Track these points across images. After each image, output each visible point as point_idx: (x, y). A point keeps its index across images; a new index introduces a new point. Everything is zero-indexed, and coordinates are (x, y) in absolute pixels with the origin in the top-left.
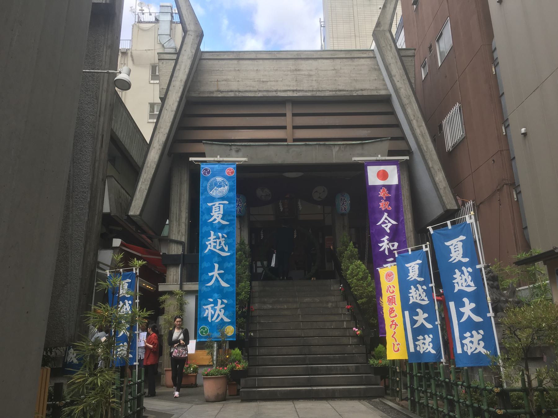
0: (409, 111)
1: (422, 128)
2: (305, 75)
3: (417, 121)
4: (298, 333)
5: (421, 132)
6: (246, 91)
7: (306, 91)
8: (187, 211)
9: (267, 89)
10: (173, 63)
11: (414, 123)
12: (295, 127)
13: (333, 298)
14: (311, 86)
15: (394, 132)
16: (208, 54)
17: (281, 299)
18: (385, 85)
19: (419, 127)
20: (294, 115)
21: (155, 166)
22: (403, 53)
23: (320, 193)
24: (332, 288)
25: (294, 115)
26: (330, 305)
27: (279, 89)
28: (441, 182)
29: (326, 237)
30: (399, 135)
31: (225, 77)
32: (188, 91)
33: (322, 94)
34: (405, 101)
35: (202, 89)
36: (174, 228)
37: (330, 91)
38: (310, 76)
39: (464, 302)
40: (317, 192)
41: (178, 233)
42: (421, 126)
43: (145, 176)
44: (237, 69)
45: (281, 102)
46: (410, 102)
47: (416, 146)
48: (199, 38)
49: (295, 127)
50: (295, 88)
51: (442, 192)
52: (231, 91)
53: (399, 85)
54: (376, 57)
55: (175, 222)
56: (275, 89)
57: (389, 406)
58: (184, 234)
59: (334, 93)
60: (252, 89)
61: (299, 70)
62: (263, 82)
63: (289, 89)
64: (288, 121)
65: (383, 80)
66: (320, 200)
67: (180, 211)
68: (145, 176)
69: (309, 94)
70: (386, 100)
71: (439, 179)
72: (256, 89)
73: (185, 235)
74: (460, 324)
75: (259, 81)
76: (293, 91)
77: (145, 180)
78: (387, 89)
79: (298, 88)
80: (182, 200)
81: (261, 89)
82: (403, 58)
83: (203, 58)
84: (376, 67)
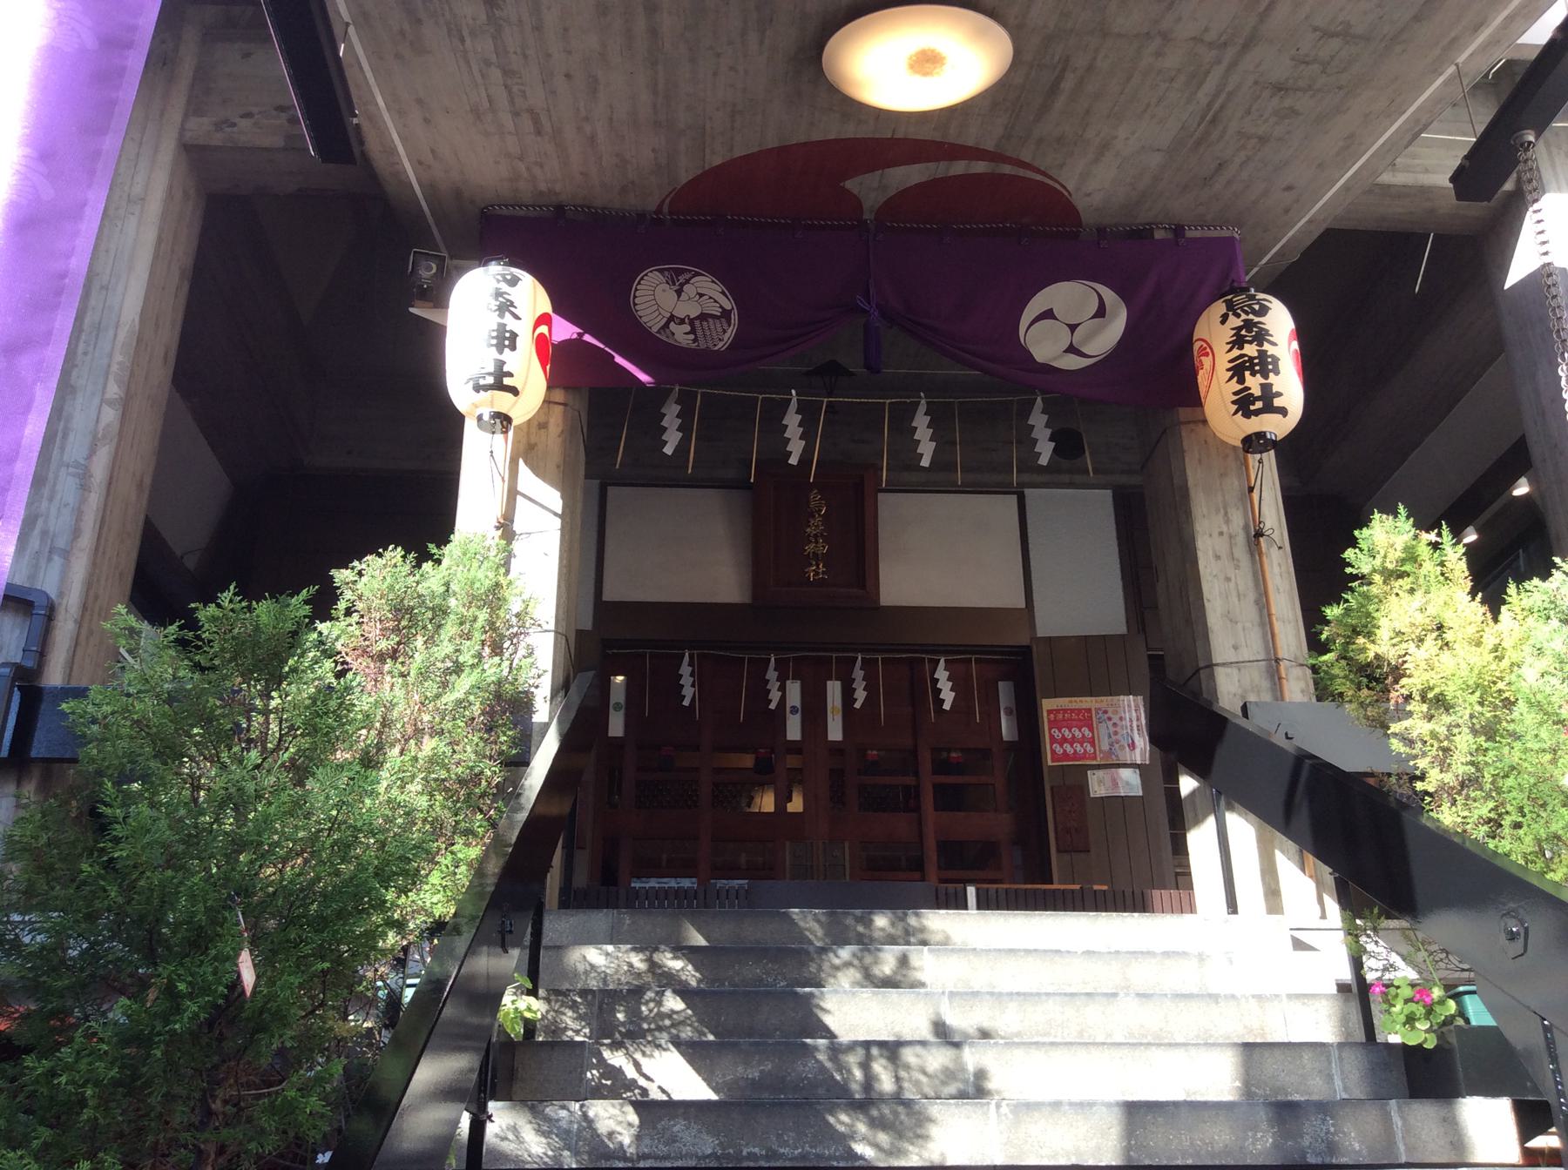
29: (1048, 704)
40: (1048, 314)
66: (1073, 363)
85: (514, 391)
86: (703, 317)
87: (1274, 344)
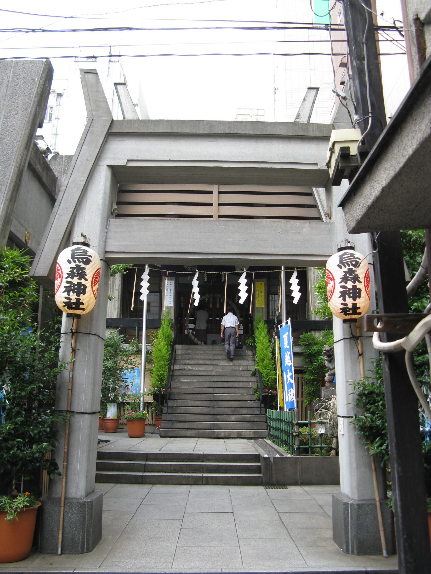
4: (210, 390)
8: (120, 279)
12: (220, 204)
24: (246, 353)
25: (220, 192)
30: (317, 215)
49: (220, 204)
58: (117, 299)
64: (215, 198)
73: (118, 301)
85: (83, 309)
87: (86, 280)
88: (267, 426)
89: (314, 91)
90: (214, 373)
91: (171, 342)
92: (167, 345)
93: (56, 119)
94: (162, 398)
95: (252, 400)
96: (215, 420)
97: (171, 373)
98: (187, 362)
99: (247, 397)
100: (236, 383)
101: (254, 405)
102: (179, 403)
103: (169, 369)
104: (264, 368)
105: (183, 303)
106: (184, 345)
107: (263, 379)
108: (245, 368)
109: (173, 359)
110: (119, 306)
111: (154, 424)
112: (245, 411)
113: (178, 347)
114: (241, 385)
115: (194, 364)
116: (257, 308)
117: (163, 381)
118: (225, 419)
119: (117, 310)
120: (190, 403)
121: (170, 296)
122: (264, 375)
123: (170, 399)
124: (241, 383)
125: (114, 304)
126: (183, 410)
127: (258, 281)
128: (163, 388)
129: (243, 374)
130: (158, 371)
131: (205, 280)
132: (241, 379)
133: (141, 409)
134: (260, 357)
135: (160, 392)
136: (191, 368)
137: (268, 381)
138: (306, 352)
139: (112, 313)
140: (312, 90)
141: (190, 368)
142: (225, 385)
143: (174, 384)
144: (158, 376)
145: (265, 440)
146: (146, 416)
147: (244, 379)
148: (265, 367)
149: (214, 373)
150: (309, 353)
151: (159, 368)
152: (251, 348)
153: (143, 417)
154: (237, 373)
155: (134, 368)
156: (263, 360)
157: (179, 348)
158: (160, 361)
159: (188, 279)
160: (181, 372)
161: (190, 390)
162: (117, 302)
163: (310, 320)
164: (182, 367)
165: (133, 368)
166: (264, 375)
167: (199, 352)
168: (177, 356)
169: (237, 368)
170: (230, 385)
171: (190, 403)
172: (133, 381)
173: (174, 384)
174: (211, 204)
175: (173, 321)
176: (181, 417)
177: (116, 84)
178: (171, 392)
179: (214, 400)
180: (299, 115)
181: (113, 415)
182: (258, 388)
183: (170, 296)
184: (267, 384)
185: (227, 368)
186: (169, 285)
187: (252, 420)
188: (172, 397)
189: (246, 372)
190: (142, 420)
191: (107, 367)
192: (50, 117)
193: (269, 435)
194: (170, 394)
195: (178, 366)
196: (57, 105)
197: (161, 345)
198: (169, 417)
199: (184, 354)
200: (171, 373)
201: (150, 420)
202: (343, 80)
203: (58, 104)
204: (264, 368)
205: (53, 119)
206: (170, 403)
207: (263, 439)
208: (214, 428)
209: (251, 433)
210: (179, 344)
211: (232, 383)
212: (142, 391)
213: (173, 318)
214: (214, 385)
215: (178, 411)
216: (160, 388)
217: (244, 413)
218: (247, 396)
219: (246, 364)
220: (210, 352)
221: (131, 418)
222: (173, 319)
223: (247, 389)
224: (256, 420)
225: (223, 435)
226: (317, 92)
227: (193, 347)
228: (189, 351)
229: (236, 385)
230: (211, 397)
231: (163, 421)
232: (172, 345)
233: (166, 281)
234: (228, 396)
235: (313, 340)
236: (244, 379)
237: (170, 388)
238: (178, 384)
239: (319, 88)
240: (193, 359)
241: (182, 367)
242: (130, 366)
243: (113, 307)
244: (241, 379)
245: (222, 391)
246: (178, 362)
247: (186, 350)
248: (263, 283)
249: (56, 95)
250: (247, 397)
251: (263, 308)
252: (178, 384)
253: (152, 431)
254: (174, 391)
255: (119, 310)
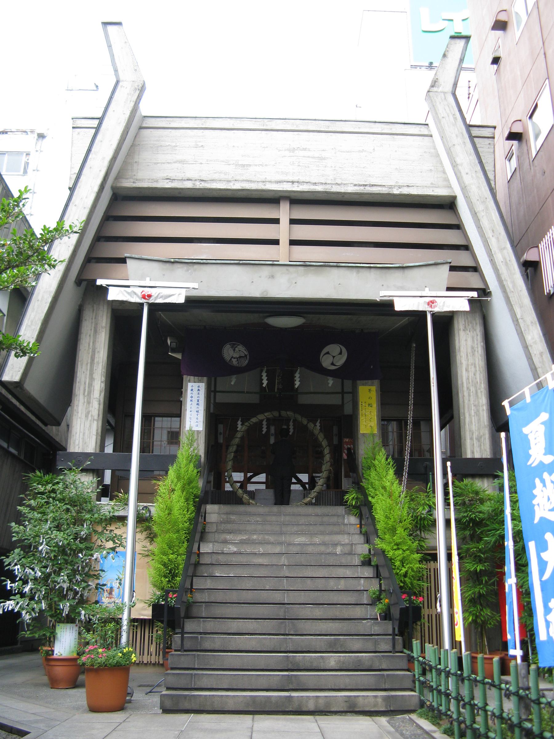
0: (485, 223)
1: (505, 251)
2: (313, 158)
3: (498, 239)
4: (277, 597)
5: (505, 258)
6: (213, 180)
7: (315, 184)
8: (103, 379)
9: (248, 178)
10: (93, 131)
11: (493, 242)
12: (293, 243)
13: (345, 539)
14: (323, 176)
15: (462, 259)
16: (154, 119)
17: (255, 537)
18: (447, 180)
19: (502, 249)
20: (293, 222)
21: (50, 300)
22: (475, 132)
23: (334, 356)
24: (346, 521)
25: (293, 222)
26: (338, 550)
27: (269, 179)
28: (535, 343)
30: (471, 263)
31: (179, 157)
32: (117, 178)
33: (342, 189)
34: (479, 208)
35: (140, 175)
36: (80, 408)
37: (355, 185)
38: (322, 159)
39: (546, 542)
40: (328, 353)
41: (87, 416)
42: (504, 248)
43: (32, 316)
44: (200, 144)
45: (272, 199)
46: (487, 208)
47: (496, 283)
48: (138, 92)
49: (293, 243)
50: (295, 179)
51: (536, 360)
52: (189, 180)
53: (467, 180)
54: (431, 136)
55: (81, 397)
56: (262, 178)
57: (421, 728)
58: (96, 418)
59: (362, 188)
60: (222, 177)
61: (305, 149)
62: (243, 166)
63: (286, 179)
64: (283, 231)
65: (444, 172)
66: (333, 368)
67: (92, 379)
68: (32, 316)
69: (319, 188)
70: (448, 205)
71: (533, 339)
72: (230, 178)
73: (98, 421)
74: (544, 585)
75: (237, 165)
76: (293, 182)
77: (32, 322)
78: (450, 187)
79: (302, 179)
80: (96, 360)
81: (237, 178)
82: (475, 139)
83: (144, 125)
84: (433, 151)
86: (240, 357)
88: (414, 682)
89: (462, 42)
90: (284, 560)
91: (196, 496)
92: (187, 500)
93: (34, 170)
94: (169, 616)
95: (370, 620)
96: (290, 667)
97: (194, 559)
98: (228, 537)
99: (358, 612)
100: (331, 580)
101: (376, 629)
102: (210, 626)
103: (189, 552)
104: (395, 547)
105: (222, 436)
106: (222, 506)
107: (394, 571)
108: (347, 549)
109: (197, 531)
110: (100, 431)
111: (161, 662)
112: (356, 644)
113: (210, 508)
114: (342, 584)
115: (242, 542)
116: (363, 434)
117: (174, 576)
118: (315, 665)
119: (94, 438)
120: (234, 626)
121: (197, 412)
122: (398, 563)
123: (189, 616)
124: (342, 581)
125: (90, 426)
126: (217, 642)
127: (363, 385)
128: (174, 592)
129: (344, 561)
130: (165, 554)
131: (264, 386)
132: (341, 572)
133: (124, 639)
134: (386, 523)
135: (165, 600)
136: (235, 549)
137: (405, 575)
138: (464, 517)
139: (85, 443)
140: (458, 41)
141: (234, 549)
142: (309, 584)
143: (198, 583)
144: (165, 565)
145: (414, 716)
146: (129, 659)
147: (348, 572)
148: (397, 544)
149: (284, 560)
150: (471, 519)
151: (165, 546)
152: (355, 511)
153: (123, 663)
154: (331, 560)
155: (117, 549)
156: (393, 531)
157: (213, 511)
158: (168, 531)
159: (232, 383)
160: (215, 557)
161: (234, 596)
162: (95, 422)
163: (463, 457)
164: (218, 548)
165: (113, 549)
166: (398, 563)
167: (253, 519)
168: (207, 526)
169: (330, 550)
170: (320, 584)
171: (234, 626)
172: (121, 576)
173: (198, 583)
174: (276, 242)
175: (203, 459)
176: (213, 659)
177: (105, 24)
178: (191, 600)
179: (286, 619)
180: (435, 82)
181: (68, 649)
182: (381, 591)
183: (197, 412)
184: (404, 582)
185: (310, 549)
186: (195, 392)
187: (376, 666)
188: (195, 611)
189: (349, 557)
190: (122, 669)
191: (57, 545)
192: (25, 168)
193: (422, 704)
194: (189, 606)
195: (211, 545)
196: (37, 151)
197: (172, 497)
198: (185, 660)
199: (221, 523)
200: (194, 559)
201: (154, 654)
202: (497, 55)
203: (38, 149)
204: (395, 547)
205: (29, 170)
206: (190, 626)
207: (406, 716)
208: (291, 687)
209: (380, 700)
210: (213, 503)
211: (324, 580)
212: (126, 599)
213: (202, 452)
214: (285, 584)
215: (207, 645)
216: (167, 592)
217: (356, 647)
218: (358, 608)
219: (347, 541)
220: (274, 518)
221: (92, 665)
222: (203, 456)
223: (356, 594)
224: (384, 667)
225: (311, 706)
226: (467, 43)
227: (241, 508)
228: (233, 517)
229: (332, 584)
230: (280, 612)
231: (172, 669)
232: (200, 503)
233: (190, 385)
234: (317, 610)
235: (477, 493)
236: (348, 572)
237: (191, 590)
238: (209, 584)
239: (470, 37)
240: (239, 532)
241: (218, 548)
242: (110, 544)
243: (87, 432)
244: (341, 572)
245: (302, 597)
246: (210, 537)
247: (227, 514)
248: (374, 388)
249: (36, 136)
250: (358, 612)
251: (374, 435)
252: (209, 584)
253: (129, 715)
254: (199, 597)
255: (99, 438)
